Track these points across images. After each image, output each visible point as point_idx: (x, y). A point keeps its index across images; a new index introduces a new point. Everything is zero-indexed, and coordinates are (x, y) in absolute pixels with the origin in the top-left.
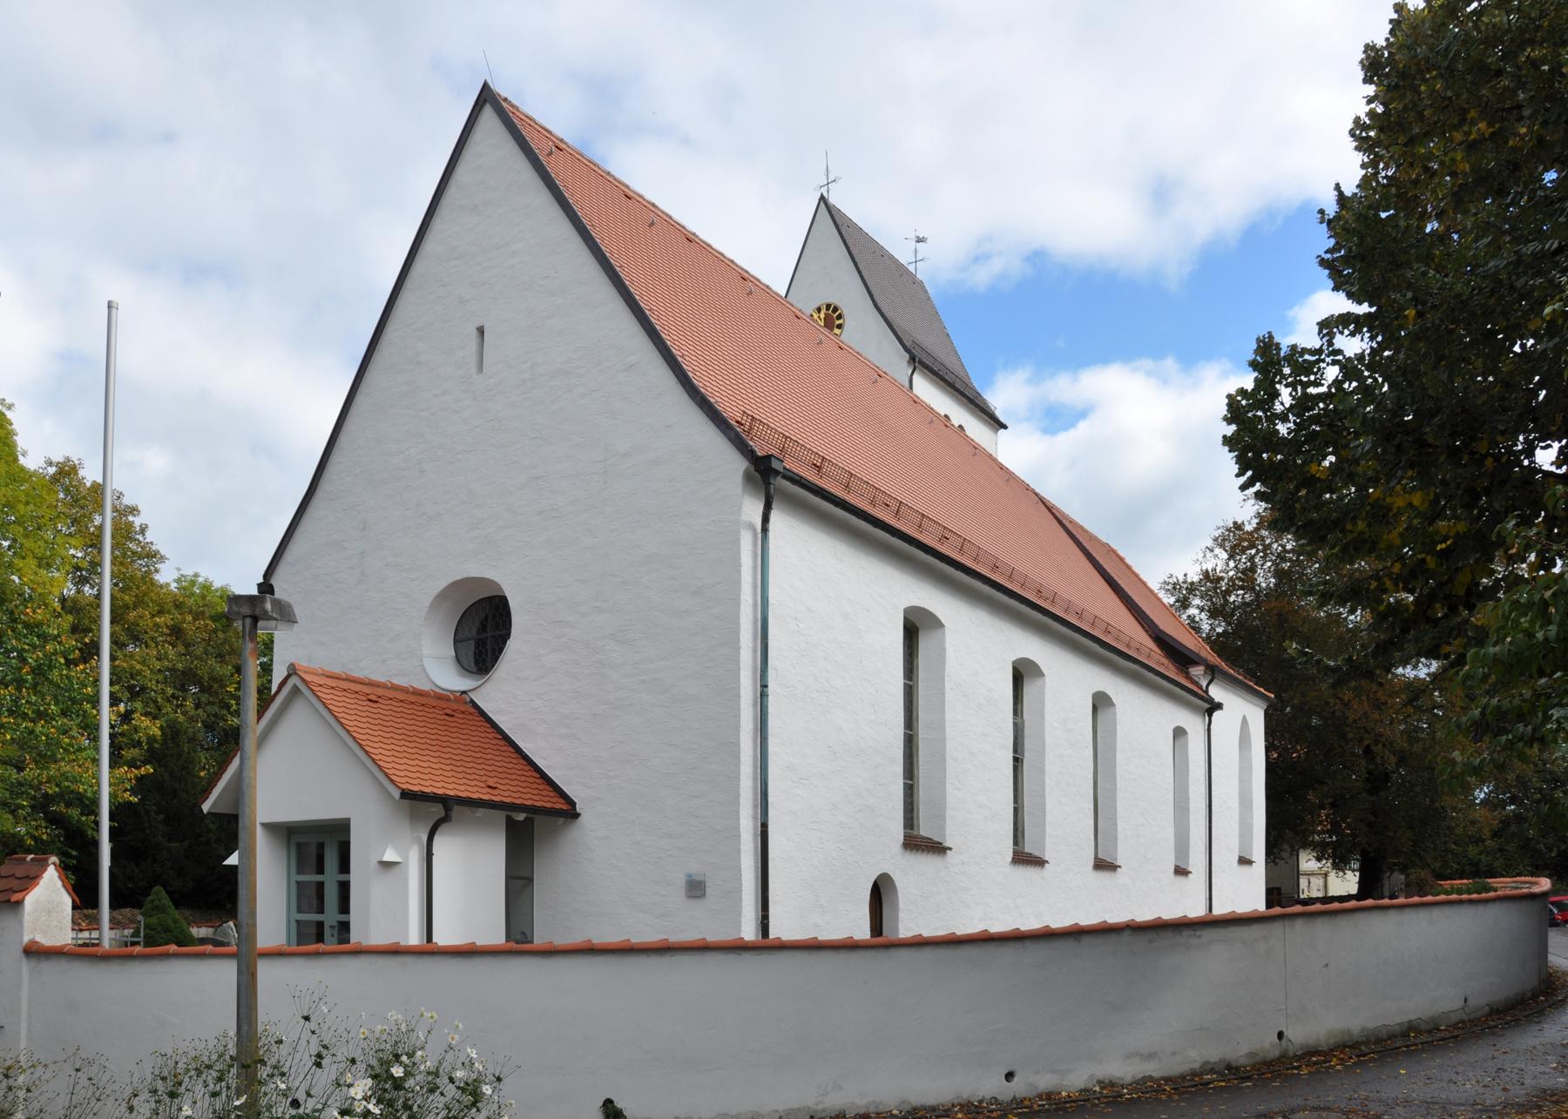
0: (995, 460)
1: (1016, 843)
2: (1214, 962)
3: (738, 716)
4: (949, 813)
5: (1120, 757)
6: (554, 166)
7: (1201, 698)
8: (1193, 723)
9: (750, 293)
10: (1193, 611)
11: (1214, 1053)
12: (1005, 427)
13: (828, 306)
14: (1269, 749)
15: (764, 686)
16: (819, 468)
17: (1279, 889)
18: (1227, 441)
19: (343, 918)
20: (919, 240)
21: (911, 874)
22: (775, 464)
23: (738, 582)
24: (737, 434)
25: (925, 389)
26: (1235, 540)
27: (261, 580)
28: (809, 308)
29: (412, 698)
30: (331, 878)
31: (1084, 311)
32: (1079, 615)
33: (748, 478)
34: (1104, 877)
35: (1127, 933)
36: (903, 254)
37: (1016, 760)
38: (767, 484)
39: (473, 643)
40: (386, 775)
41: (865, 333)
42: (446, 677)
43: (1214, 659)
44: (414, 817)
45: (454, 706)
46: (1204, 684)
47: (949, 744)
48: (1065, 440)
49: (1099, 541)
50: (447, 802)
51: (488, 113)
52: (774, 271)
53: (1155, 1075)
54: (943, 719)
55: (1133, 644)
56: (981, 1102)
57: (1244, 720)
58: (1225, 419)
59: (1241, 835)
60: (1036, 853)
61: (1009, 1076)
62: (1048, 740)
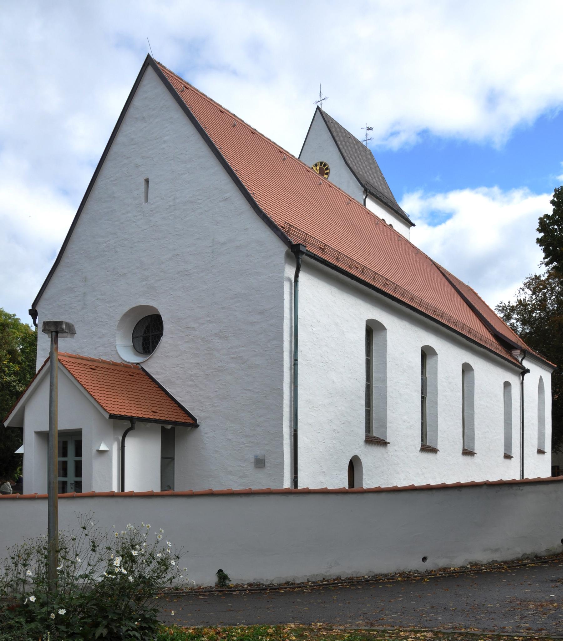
0: (410, 243)
1: (422, 441)
2: (530, 501)
3: (282, 375)
4: (389, 425)
5: (476, 397)
6: (185, 97)
7: (518, 367)
8: (514, 380)
9: (284, 159)
10: (513, 321)
11: (529, 549)
12: (414, 225)
13: (321, 163)
14: (553, 393)
15: (296, 360)
16: (323, 250)
17: (558, 467)
18: (539, 241)
19: (78, 479)
20: (369, 129)
21: (370, 458)
22: (302, 248)
23: (283, 308)
24: (282, 233)
25: (372, 206)
26: (535, 284)
27: (31, 308)
28: (311, 164)
29: (113, 367)
30: (71, 459)
31: (453, 161)
32: (455, 323)
33: (288, 255)
34: (468, 459)
35: (485, 487)
36: (359, 135)
37: (422, 398)
38: (298, 258)
39: (141, 338)
40: (102, 406)
41: (341, 177)
42: (128, 356)
43: (525, 346)
44: (115, 428)
45: (134, 371)
46: (520, 359)
47: (389, 390)
48: (442, 230)
49: (464, 284)
50: (132, 420)
51: (150, 70)
52: (292, 144)
53: (498, 560)
54: (385, 377)
55: (483, 338)
56: (410, 572)
57: (541, 378)
58: (538, 230)
59: (505, 446)
60: (433, 446)
61: (424, 559)
62: (439, 387)
